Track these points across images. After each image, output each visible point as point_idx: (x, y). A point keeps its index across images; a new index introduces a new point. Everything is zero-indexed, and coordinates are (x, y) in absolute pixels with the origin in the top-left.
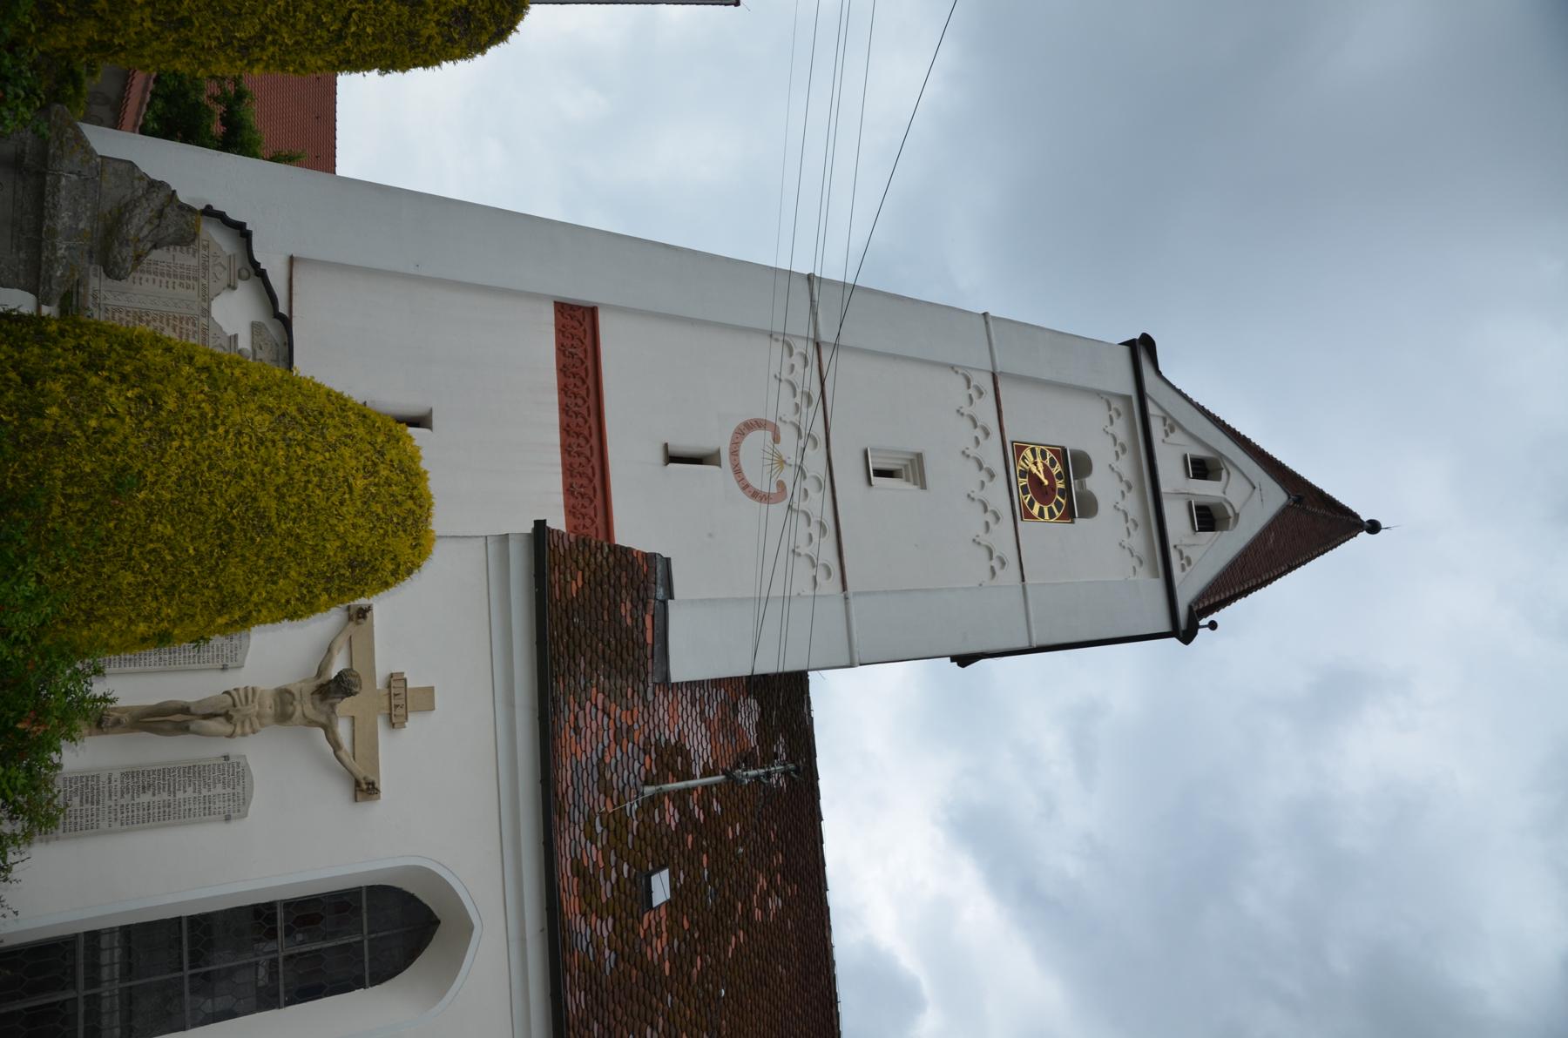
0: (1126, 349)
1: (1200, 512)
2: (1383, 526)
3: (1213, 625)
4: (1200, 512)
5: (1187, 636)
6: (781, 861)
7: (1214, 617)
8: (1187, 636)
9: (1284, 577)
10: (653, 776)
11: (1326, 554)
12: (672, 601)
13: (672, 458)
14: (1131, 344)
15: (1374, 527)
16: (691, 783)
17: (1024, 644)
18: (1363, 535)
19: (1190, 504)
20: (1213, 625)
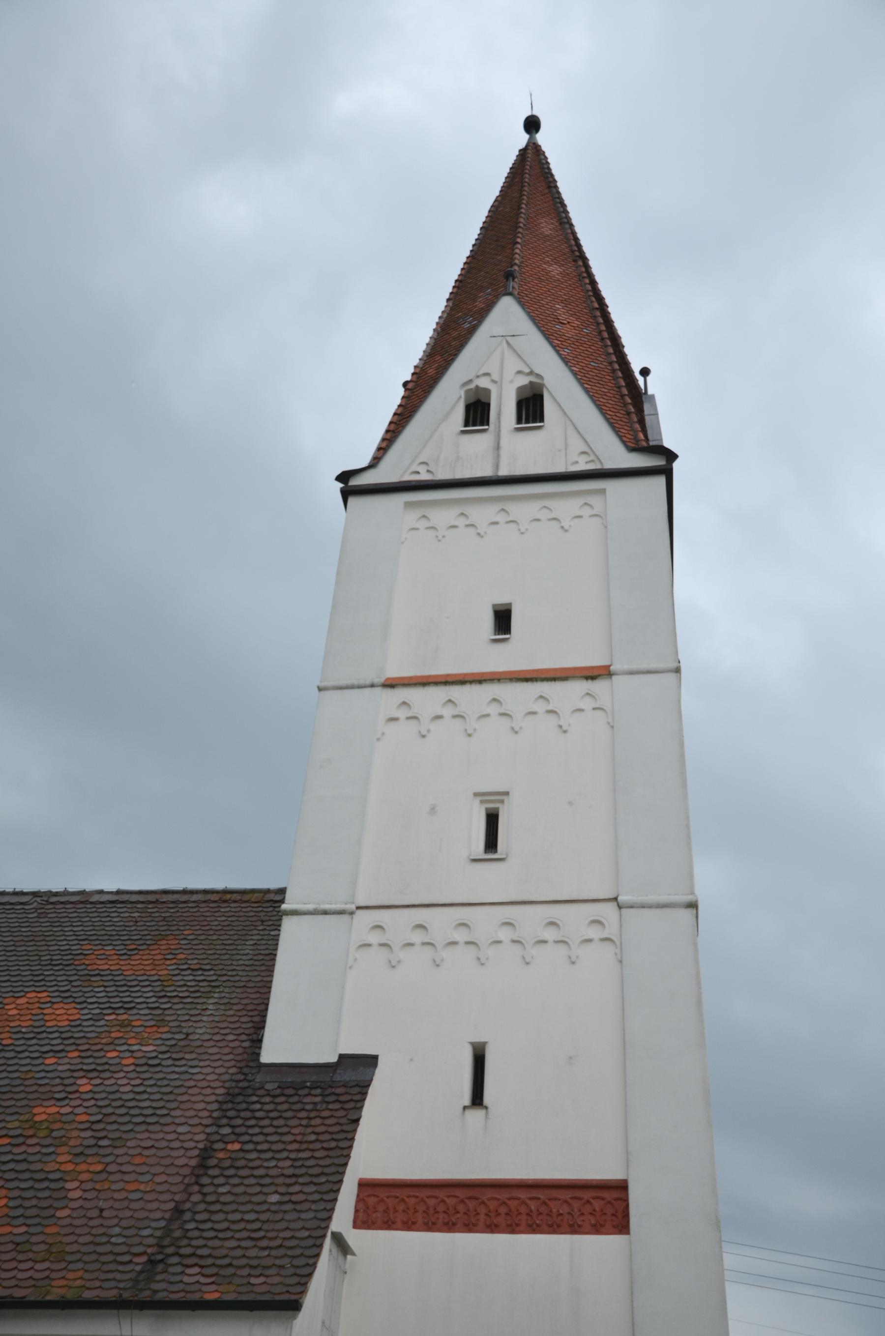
0: (352, 500)
1: (478, 422)
2: (529, 114)
3: (645, 372)
4: (478, 422)
5: (671, 456)
6: (466, 327)
7: (636, 368)
8: (671, 456)
9: (610, 309)
10: (233, 1133)
11: (566, 202)
12: (288, 896)
13: (477, 1098)
14: (346, 494)
15: (532, 125)
16: (391, 1213)
17: (486, 471)
18: (541, 138)
19: (463, 432)
20: (645, 372)
